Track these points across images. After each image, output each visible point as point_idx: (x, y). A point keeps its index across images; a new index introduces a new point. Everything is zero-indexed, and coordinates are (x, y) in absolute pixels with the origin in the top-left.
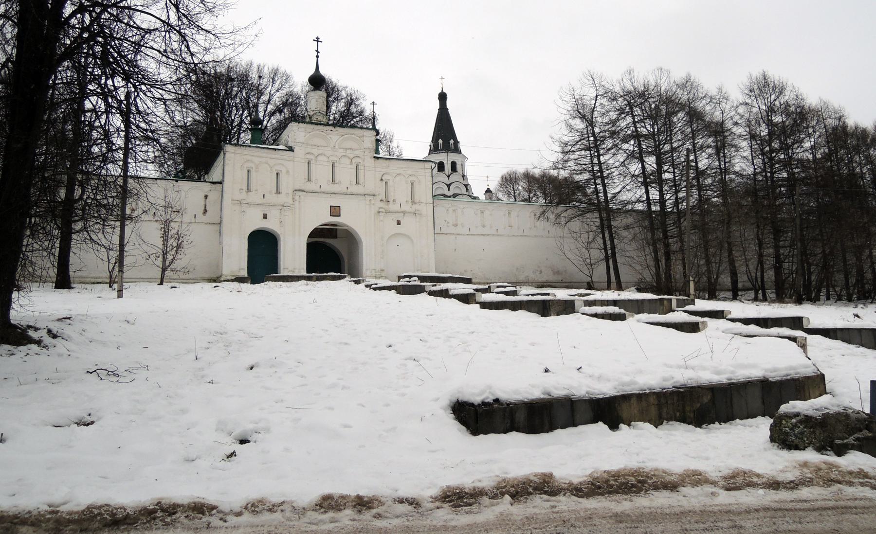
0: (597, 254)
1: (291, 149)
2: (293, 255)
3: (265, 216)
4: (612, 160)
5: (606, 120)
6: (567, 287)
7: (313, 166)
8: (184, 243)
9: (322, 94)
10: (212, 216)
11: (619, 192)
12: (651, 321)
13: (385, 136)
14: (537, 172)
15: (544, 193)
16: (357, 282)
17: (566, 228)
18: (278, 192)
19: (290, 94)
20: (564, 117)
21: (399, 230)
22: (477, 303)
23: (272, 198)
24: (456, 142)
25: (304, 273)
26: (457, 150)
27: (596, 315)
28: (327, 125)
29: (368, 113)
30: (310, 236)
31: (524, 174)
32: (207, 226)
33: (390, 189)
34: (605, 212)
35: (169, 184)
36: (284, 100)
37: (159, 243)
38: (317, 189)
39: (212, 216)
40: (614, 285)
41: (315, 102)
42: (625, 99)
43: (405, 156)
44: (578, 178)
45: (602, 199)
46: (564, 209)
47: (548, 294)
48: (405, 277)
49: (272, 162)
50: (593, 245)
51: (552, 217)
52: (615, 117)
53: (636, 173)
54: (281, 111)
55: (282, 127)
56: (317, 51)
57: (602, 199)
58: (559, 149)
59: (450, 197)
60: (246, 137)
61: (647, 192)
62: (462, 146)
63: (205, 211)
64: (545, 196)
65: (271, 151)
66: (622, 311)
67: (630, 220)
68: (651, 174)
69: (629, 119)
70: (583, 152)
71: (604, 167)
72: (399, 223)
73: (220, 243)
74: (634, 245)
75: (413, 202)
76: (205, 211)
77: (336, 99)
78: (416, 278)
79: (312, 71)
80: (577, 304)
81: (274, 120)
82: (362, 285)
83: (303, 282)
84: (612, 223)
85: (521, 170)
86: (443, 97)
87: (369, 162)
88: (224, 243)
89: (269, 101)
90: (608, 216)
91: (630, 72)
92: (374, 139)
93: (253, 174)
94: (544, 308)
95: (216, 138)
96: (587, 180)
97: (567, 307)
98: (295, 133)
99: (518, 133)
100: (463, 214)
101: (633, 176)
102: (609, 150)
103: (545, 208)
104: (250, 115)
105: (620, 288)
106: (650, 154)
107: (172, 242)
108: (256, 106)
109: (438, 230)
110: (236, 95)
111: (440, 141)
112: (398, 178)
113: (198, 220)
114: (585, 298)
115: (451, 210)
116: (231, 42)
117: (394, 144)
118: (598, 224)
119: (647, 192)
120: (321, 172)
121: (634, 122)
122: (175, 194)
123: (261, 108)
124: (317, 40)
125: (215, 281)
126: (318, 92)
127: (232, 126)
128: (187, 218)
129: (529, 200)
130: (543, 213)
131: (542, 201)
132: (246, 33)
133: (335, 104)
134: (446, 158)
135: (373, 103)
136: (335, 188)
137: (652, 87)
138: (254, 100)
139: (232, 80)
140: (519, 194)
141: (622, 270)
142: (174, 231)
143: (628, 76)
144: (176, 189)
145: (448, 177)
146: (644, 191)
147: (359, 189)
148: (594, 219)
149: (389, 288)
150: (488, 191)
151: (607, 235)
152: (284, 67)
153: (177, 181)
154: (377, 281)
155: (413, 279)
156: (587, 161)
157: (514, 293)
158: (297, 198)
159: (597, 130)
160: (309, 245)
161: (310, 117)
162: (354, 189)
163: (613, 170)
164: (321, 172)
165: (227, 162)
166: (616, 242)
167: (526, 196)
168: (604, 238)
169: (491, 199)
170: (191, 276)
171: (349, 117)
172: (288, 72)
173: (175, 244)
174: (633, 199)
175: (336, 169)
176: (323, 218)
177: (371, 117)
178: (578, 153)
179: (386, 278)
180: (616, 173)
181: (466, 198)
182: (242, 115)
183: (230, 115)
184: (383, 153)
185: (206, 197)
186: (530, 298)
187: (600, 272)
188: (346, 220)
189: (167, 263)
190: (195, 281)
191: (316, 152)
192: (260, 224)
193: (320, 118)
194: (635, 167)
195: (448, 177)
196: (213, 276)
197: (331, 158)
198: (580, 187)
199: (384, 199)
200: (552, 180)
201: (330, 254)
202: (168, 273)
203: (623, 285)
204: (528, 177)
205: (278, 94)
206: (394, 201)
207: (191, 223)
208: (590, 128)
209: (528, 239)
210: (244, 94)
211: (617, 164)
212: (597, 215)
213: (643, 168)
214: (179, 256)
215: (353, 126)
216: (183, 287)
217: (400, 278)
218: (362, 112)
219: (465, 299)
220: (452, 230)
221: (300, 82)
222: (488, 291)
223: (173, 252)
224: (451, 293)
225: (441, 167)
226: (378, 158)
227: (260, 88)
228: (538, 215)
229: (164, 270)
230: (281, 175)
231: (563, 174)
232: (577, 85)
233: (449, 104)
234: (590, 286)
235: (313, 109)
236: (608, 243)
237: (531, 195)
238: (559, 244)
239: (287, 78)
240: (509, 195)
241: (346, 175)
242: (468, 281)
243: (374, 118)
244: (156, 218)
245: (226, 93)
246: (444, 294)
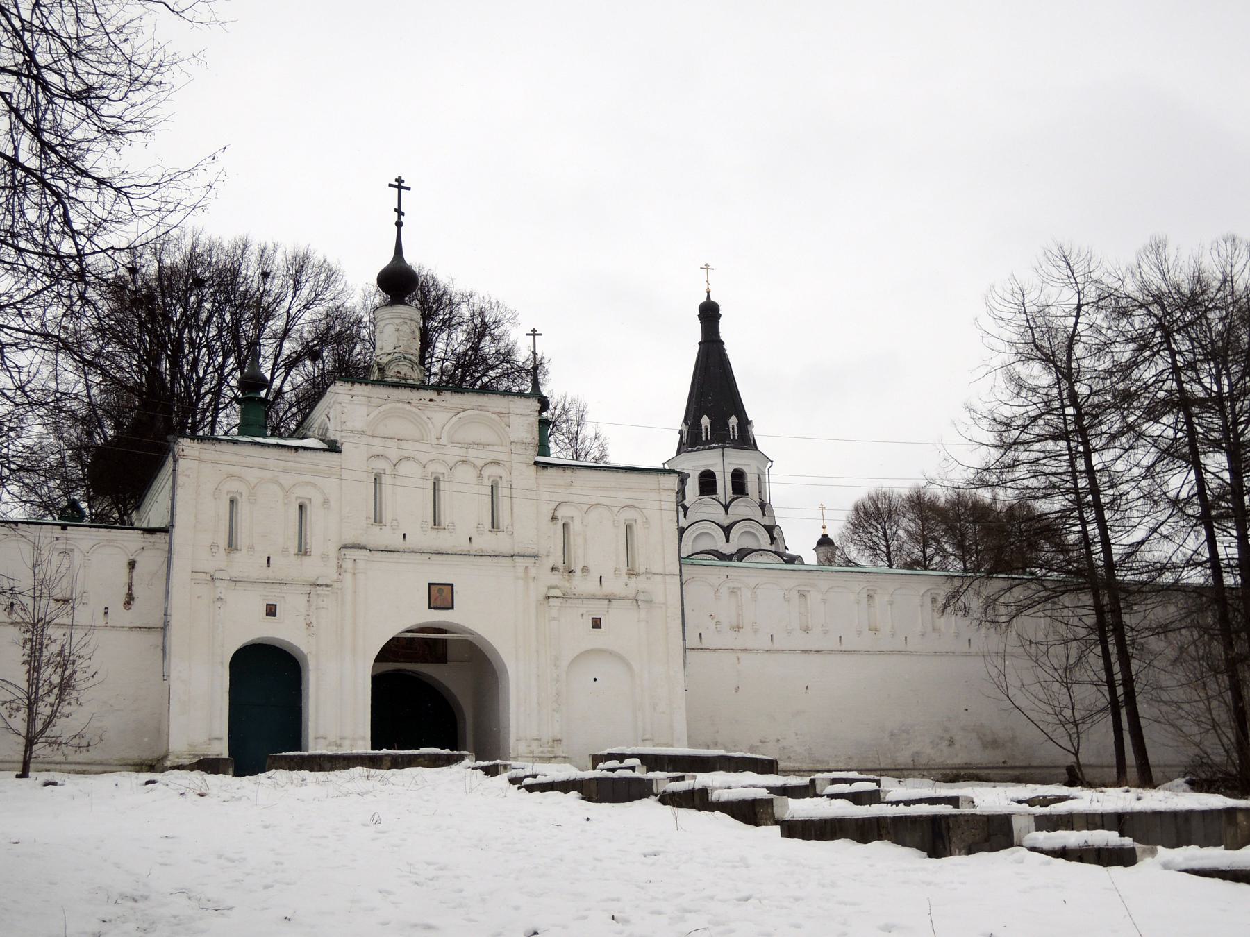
0: (1091, 696)
1: (334, 447)
2: (339, 705)
3: (271, 611)
4: (1123, 462)
5: (1105, 364)
6: (1018, 780)
7: (386, 491)
8: (78, 676)
9: (409, 314)
10: (145, 610)
11: (1143, 542)
12: (1196, 865)
13: (565, 411)
14: (941, 493)
15: (960, 545)
16: (491, 771)
17: (1013, 635)
18: (302, 551)
19: (336, 315)
20: (999, 360)
21: (597, 639)
22: (776, 823)
23: (288, 566)
24: (744, 423)
25: (364, 747)
26: (745, 441)
27: (1064, 853)
28: (422, 386)
29: (522, 356)
30: (381, 658)
31: (910, 499)
32: (135, 635)
33: (576, 541)
34: (1107, 593)
35: (46, 534)
36: (322, 327)
37: (20, 676)
38: (397, 542)
39: (145, 610)
40: (1132, 773)
41: (393, 333)
42: (1150, 313)
43: (614, 460)
44: (1042, 506)
45: (1099, 558)
46: (1005, 584)
47: (954, 801)
48: (610, 757)
49: (287, 480)
50: (1079, 674)
51: (976, 605)
52: (1127, 356)
53: (1183, 495)
54: (315, 356)
55: (312, 396)
56: (399, 212)
57: (1099, 558)
58: (991, 438)
59: (729, 557)
60: (229, 418)
61: (1211, 542)
62: (757, 431)
63: (130, 599)
64: (963, 550)
65: (284, 452)
66: (1128, 841)
67: (1169, 611)
68: (1221, 497)
69: (1161, 364)
70: (1050, 445)
71: (1102, 479)
72: (596, 623)
73: (165, 677)
74: (1180, 674)
75: (632, 573)
76: (130, 599)
77: (447, 324)
78: (636, 762)
80: (1017, 824)
81: (297, 377)
82: (502, 780)
83: (359, 771)
84: (1126, 619)
85: (901, 486)
86: (709, 314)
87: (525, 475)
88: (174, 675)
89: (286, 331)
90: (1115, 601)
91: (1158, 247)
92: (534, 419)
93: (243, 509)
94: (936, 836)
95: (160, 425)
96: (1064, 514)
97: (994, 834)
98: (346, 407)
99: (893, 399)
100: (761, 596)
101: (1174, 502)
102: (1114, 437)
103: (957, 583)
104: (240, 365)
105: (1147, 780)
106: (1216, 446)
107: (50, 675)
108: (254, 344)
109: (692, 641)
110: (209, 319)
111: (705, 421)
112: (594, 514)
113: (113, 619)
114: (1038, 810)
115: (724, 591)
116: (155, 205)
117: (587, 432)
118: (1091, 620)
119: (1211, 542)
120: (407, 503)
121: (1176, 369)
122: (56, 559)
123: (267, 348)
124: (399, 185)
125: (152, 768)
126: (400, 309)
127: (198, 394)
128: (83, 616)
129: (922, 563)
130: (955, 595)
131: (955, 566)
132: (191, 182)
133: (444, 336)
134: (721, 462)
135: (534, 333)
136: (442, 540)
137: (1216, 284)
138: (247, 328)
139: (199, 283)
140: (900, 549)
141: (1151, 734)
142: (54, 648)
143: (1152, 257)
144: (60, 545)
145: (726, 508)
146: (1203, 537)
147: (499, 543)
148: (1079, 610)
149: (564, 786)
150: (825, 541)
151: (1113, 649)
152: (322, 251)
153: (64, 527)
154: (539, 768)
155: (628, 762)
156: (1062, 465)
157: (872, 797)
158: (348, 564)
159: (1082, 389)
160: (376, 680)
161: (381, 370)
162: (487, 541)
163: (1125, 487)
164: (407, 503)
165: (181, 479)
166: (1135, 665)
167: (917, 553)
168: (1106, 656)
169: (830, 561)
170: (93, 755)
171: (478, 368)
172: (332, 261)
173: (56, 679)
174: (1178, 559)
175: (444, 497)
176: (409, 613)
177: (529, 366)
178: (1037, 446)
179: (566, 759)
180: (1134, 494)
181: (769, 560)
182: (222, 366)
183: (194, 367)
184: (558, 452)
185: (132, 564)
186: (902, 810)
187: (1099, 741)
188: (467, 616)
189: (39, 725)
190: (104, 767)
192: (254, 628)
193: (405, 370)
194: (1179, 481)
195: (726, 508)
196: (148, 755)
197: (432, 468)
198: (1048, 529)
199: (560, 564)
200: (980, 512)
201: (431, 703)
202: (39, 749)
203: (1156, 774)
204: (920, 505)
205: (308, 315)
207: (93, 628)
208: (1065, 384)
209: (893, 662)
210: (228, 318)
211: (1136, 471)
212: (1087, 599)
213: (1201, 481)
214: (66, 709)
215: (486, 390)
216: (72, 784)
217: (597, 760)
218: (509, 353)
219: (749, 812)
220: (729, 640)
221: (358, 288)
222: (808, 791)
223: (52, 699)
224: (714, 797)
225: (708, 483)
226: (545, 466)
227: (264, 303)
228: (941, 600)
229: (30, 742)
230: (310, 512)
231: (1007, 496)
232: (1029, 279)
233: (726, 330)
234: (1074, 777)
235: (389, 349)
236: (1116, 668)
237: (930, 551)
238: (994, 673)
239: (330, 275)
240: (874, 549)
241: (466, 508)
242: (766, 767)
243: (535, 368)
244: (16, 618)
245: (184, 314)
246: (699, 800)
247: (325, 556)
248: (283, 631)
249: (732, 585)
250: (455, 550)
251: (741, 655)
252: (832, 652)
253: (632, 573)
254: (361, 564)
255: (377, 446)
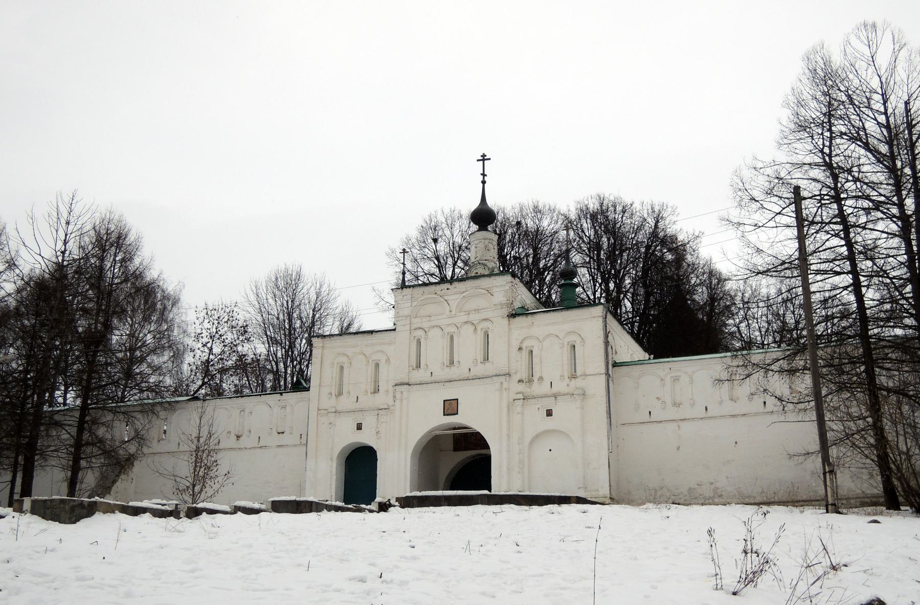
3: (359, 427)
23: (368, 401)
56: (484, 175)
72: (549, 413)
79: (475, 204)
136: (454, 372)
158: (398, 395)
186: (160, 507)
188: (470, 417)
191: (426, 325)
206: (541, 378)
220: (672, 413)
247: (387, 391)
248: (365, 438)
249: (673, 375)
250: (462, 377)
251: (681, 423)
252: (756, 414)
253: (573, 376)
254: (405, 394)
255: (417, 322)
